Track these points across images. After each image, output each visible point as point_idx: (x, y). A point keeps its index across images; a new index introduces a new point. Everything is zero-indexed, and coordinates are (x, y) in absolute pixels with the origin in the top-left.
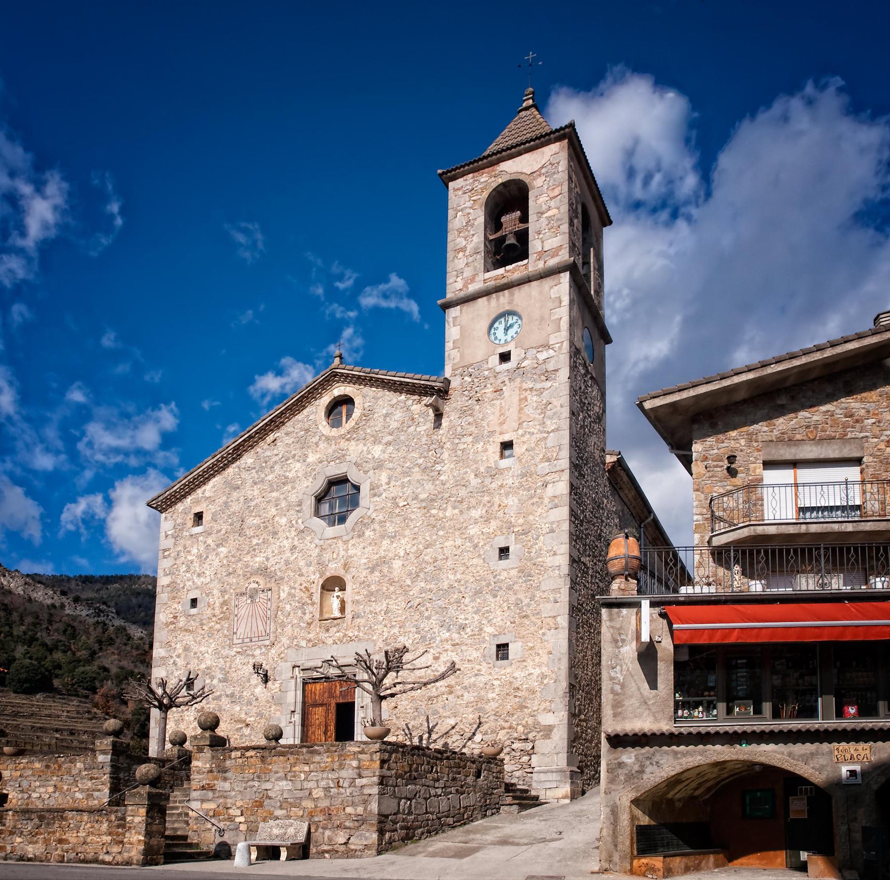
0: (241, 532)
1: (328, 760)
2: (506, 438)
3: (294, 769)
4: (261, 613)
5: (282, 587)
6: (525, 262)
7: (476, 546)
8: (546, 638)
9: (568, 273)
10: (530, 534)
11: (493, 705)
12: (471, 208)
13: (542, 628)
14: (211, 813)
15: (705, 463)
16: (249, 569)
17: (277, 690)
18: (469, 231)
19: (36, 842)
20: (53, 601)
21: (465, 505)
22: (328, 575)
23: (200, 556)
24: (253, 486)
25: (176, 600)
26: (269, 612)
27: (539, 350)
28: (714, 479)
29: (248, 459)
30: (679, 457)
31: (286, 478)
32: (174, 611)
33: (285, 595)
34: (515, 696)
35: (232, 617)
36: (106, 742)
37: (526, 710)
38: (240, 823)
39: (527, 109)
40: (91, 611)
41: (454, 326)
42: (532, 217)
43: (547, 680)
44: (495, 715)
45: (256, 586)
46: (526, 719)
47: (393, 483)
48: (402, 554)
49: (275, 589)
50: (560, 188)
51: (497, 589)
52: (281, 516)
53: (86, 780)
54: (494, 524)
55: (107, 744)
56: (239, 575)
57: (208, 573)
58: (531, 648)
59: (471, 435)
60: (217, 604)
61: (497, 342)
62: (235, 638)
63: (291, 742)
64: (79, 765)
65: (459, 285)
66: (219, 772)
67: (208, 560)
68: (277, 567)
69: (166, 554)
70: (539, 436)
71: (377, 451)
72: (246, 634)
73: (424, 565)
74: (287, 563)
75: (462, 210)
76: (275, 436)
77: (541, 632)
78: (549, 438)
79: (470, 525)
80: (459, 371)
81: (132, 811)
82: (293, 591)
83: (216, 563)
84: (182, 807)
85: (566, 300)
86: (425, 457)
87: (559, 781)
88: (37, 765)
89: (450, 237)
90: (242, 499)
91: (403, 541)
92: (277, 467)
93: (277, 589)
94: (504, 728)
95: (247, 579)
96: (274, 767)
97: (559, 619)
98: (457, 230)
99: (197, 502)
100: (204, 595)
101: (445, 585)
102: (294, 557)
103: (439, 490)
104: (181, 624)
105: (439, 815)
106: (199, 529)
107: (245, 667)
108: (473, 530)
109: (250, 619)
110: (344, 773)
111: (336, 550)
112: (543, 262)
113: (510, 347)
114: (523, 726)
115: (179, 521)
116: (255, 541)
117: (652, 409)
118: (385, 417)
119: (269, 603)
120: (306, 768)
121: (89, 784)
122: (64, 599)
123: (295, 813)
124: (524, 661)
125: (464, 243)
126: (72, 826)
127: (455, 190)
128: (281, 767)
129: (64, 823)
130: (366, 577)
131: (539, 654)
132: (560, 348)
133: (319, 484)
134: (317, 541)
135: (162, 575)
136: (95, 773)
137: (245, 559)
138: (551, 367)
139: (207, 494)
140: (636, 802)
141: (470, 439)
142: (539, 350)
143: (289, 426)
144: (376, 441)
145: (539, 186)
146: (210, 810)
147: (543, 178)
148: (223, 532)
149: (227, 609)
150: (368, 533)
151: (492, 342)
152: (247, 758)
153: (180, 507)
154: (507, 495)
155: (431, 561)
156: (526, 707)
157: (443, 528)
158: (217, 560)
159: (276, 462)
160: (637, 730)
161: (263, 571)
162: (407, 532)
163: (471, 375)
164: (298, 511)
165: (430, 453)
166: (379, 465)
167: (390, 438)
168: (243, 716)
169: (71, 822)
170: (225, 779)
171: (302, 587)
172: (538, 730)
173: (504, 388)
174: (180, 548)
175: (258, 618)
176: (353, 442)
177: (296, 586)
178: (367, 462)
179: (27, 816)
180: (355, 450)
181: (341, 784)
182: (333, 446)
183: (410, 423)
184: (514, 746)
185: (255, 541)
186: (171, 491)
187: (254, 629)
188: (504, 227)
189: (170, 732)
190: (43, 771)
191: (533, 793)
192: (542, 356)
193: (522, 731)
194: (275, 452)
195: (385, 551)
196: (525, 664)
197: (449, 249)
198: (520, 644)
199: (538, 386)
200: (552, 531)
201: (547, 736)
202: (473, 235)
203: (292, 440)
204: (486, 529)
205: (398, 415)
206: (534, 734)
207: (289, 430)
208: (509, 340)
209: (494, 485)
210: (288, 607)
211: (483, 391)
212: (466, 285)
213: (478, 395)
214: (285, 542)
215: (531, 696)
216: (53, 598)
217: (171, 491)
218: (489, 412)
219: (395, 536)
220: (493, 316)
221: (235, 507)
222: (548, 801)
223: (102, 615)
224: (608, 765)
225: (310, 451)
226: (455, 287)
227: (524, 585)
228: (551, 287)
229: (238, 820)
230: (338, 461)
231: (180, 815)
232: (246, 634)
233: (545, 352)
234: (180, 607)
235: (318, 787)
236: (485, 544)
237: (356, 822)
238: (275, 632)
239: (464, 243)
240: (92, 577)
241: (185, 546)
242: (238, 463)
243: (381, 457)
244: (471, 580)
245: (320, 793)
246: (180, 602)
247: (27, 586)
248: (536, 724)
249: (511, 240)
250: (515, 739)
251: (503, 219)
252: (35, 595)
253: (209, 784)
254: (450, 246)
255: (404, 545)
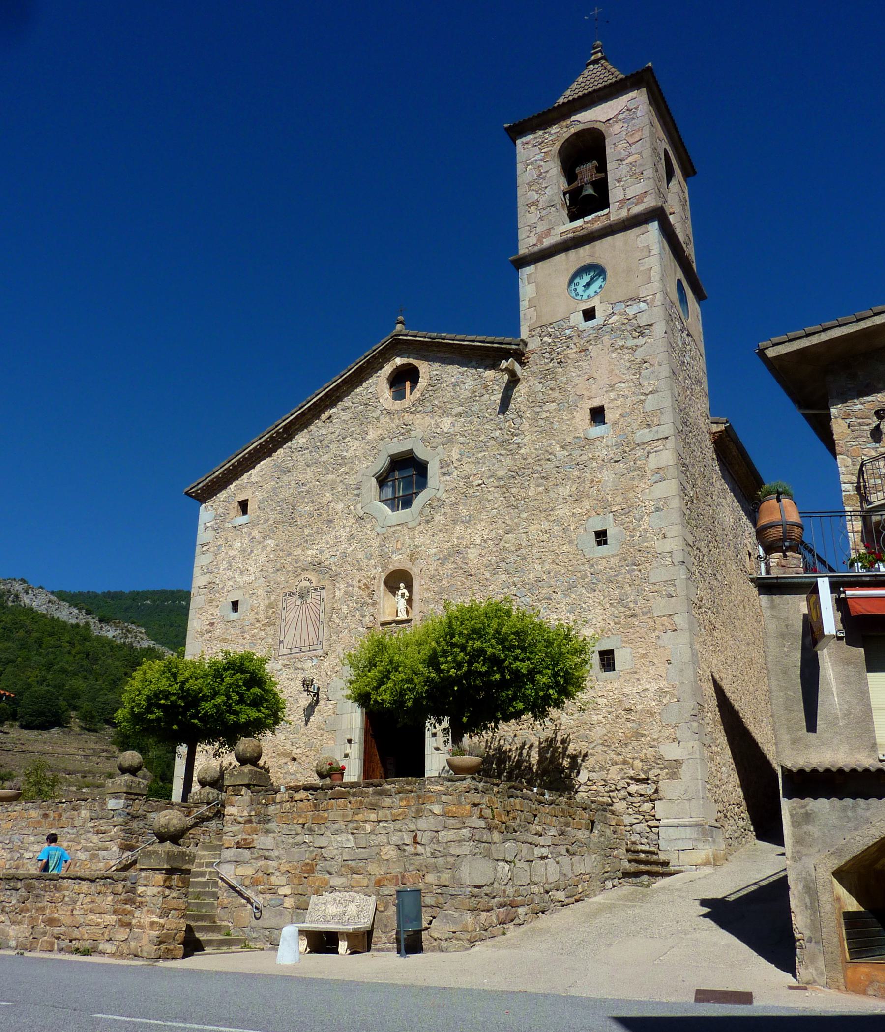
0: (292, 521)
1: (402, 804)
2: (596, 403)
3: (357, 817)
4: (313, 616)
5: (337, 585)
6: (606, 211)
7: (565, 530)
8: (660, 642)
9: (656, 223)
10: (631, 513)
11: (600, 731)
12: (541, 160)
13: (654, 630)
14: (247, 882)
15: (848, 421)
16: (300, 564)
17: (331, 712)
18: (541, 184)
19: (20, 923)
20: (78, 621)
21: (550, 484)
22: (392, 568)
23: (243, 551)
24: (305, 469)
25: (214, 603)
26: (322, 615)
27: (628, 304)
28: (862, 439)
29: (301, 439)
30: (807, 417)
31: (344, 458)
32: (211, 617)
33: (341, 594)
34: (628, 720)
35: (278, 623)
36: (119, 782)
37: (643, 739)
38: (285, 896)
39: (596, 62)
40: (119, 631)
41: (528, 283)
42: (610, 166)
43: (667, 698)
44: (603, 744)
45: (306, 583)
46: (644, 751)
47: (465, 460)
48: (478, 541)
49: (329, 586)
50: (640, 134)
51: (595, 581)
52: (339, 500)
53: (91, 834)
54: (586, 504)
55: (120, 785)
56: (289, 571)
57: (252, 570)
58: (644, 656)
59: (553, 402)
60: (262, 607)
61: (579, 298)
62: (281, 648)
63: (354, 779)
64: (85, 813)
65: (533, 240)
66: (259, 822)
67: (253, 554)
68: (333, 560)
69: (205, 548)
70: (635, 399)
71: (446, 424)
72: (295, 642)
73: (504, 555)
74: (344, 555)
75: (532, 163)
76: (331, 412)
77: (654, 635)
78: (647, 401)
79: (558, 505)
80: (537, 332)
81: (146, 878)
82: (350, 588)
83: (262, 558)
84: (211, 873)
85: (656, 249)
86: (501, 429)
87: (696, 840)
88: (34, 813)
89: (520, 191)
90: (293, 483)
91: (479, 526)
92: (333, 446)
93: (331, 586)
94: (616, 764)
95: (298, 575)
96: (331, 815)
97: (676, 618)
98: (528, 184)
99: (242, 488)
100: (247, 596)
101: (532, 577)
102: (351, 549)
103: (520, 466)
104: (218, 632)
105: (547, 887)
106: (243, 519)
107: (292, 683)
108: (562, 511)
109: (299, 624)
110: (422, 824)
111: (401, 539)
112: (626, 211)
113: (595, 302)
114: (642, 761)
115: (221, 510)
116: (307, 531)
117: (776, 358)
118: (454, 386)
119: (322, 604)
120: (373, 817)
121: (95, 838)
122: (89, 618)
123: (358, 882)
124: (636, 672)
125: (536, 196)
126: (67, 899)
127: (524, 144)
128: (339, 815)
129: (57, 895)
130: (437, 570)
131: (654, 664)
132: (653, 300)
133: (381, 462)
134: (378, 529)
135: (198, 574)
136: (102, 824)
137: (295, 553)
138: (643, 321)
139: (254, 479)
140: (839, 874)
141: (553, 406)
142: (628, 304)
143: (346, 402)
144: (445, 413)
145: (616, 133)
146: (247, 877)
147: (620, 124)
148: (271, 522)
149: (274, 612)
150: (438, 518)
151: (573, 298)
152: (296, 801)
153: (222, 495)
154: (601, 468)
155: (513, 548)
156: (643, 735)
157: (526, 510)
158: (264, 554)
159: (332, 441)
160: (827, 765)
161: (317, 566)
162: (484, 516)
163: (550, 336)
164: (358, 495)
165: (507, 424)
166: (450, 439)
167: (460, 409)
168: (288, 747)
169: (67, 893)
170: (267, 832)
171: (361, 584)
172: (662, 766)
173: (590, 348)
174: (220, 542)
175: (310, 622)
176: (418, 416)
177: (355, 582)
178: (434, 437)
179: (12, 884)
180: (422, 424)
181: (419, 840)
182: (397, 421)
183: (484, 391)
184: (630, 789)
185: (307, 531)
186: (213, 477)
187: (305, 636)
188: (579, 178)
189: (199, 770)
190: (39, 822)
191: (662, 857)
192: (631, 311)
193: (640, 768)
194: (331, 429)
195: (458, 538)
196: (637, 676)
197: (519, 204)
198: (629, 650)
199: (630, 343)
200: (658, 509)
201: (673, 776)
202: (546, 188)
203: (351, 415)
204: (578, 509)
205: (470, 383)
206: (656, 771)
207: (347, 405)
208: (592, 294)
209: (584, 458)
210: (345, 609)
211: (566, 352)
212: (540, 240)
213: (560, 357)
214: (341, 531)
215: (648, 720)
216: (77, 618)
217: (213, 477)
218: (574, 374)
219: (470, 521)
220: (573, 271)
221: (284, 494)
222: (683, 868)
223: (130, 636)
224: (792, 816)
225: (371, 426)
226: (527, 243)
227: (628, 576)
228: (638, 236)
229: (282, 891)
230: (401, 437)
231: (206, 884)
232: (295, 642)
233: (635, 307)
234: (217, 612)
235: (389, 843)
236: (577, 527)
237: (440, 897)
238: (329, 640)
239: (536, 196)
240: (122, 593)
241: (226, 539)
242: (289, 444)
243: (451, 430)
244: (563, 571)
245: (392, 852)
246: (218, 606)
247: (50, 605)
248: (659, 758)
249: (589, 191)
250: (632, 778)
251: (578, 170)
252: (59, 615)
253: (245, 840)
254: (521, 201)
255: (480, 531)
